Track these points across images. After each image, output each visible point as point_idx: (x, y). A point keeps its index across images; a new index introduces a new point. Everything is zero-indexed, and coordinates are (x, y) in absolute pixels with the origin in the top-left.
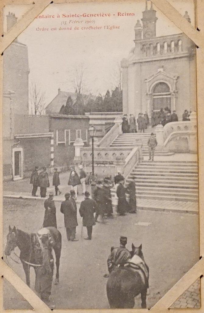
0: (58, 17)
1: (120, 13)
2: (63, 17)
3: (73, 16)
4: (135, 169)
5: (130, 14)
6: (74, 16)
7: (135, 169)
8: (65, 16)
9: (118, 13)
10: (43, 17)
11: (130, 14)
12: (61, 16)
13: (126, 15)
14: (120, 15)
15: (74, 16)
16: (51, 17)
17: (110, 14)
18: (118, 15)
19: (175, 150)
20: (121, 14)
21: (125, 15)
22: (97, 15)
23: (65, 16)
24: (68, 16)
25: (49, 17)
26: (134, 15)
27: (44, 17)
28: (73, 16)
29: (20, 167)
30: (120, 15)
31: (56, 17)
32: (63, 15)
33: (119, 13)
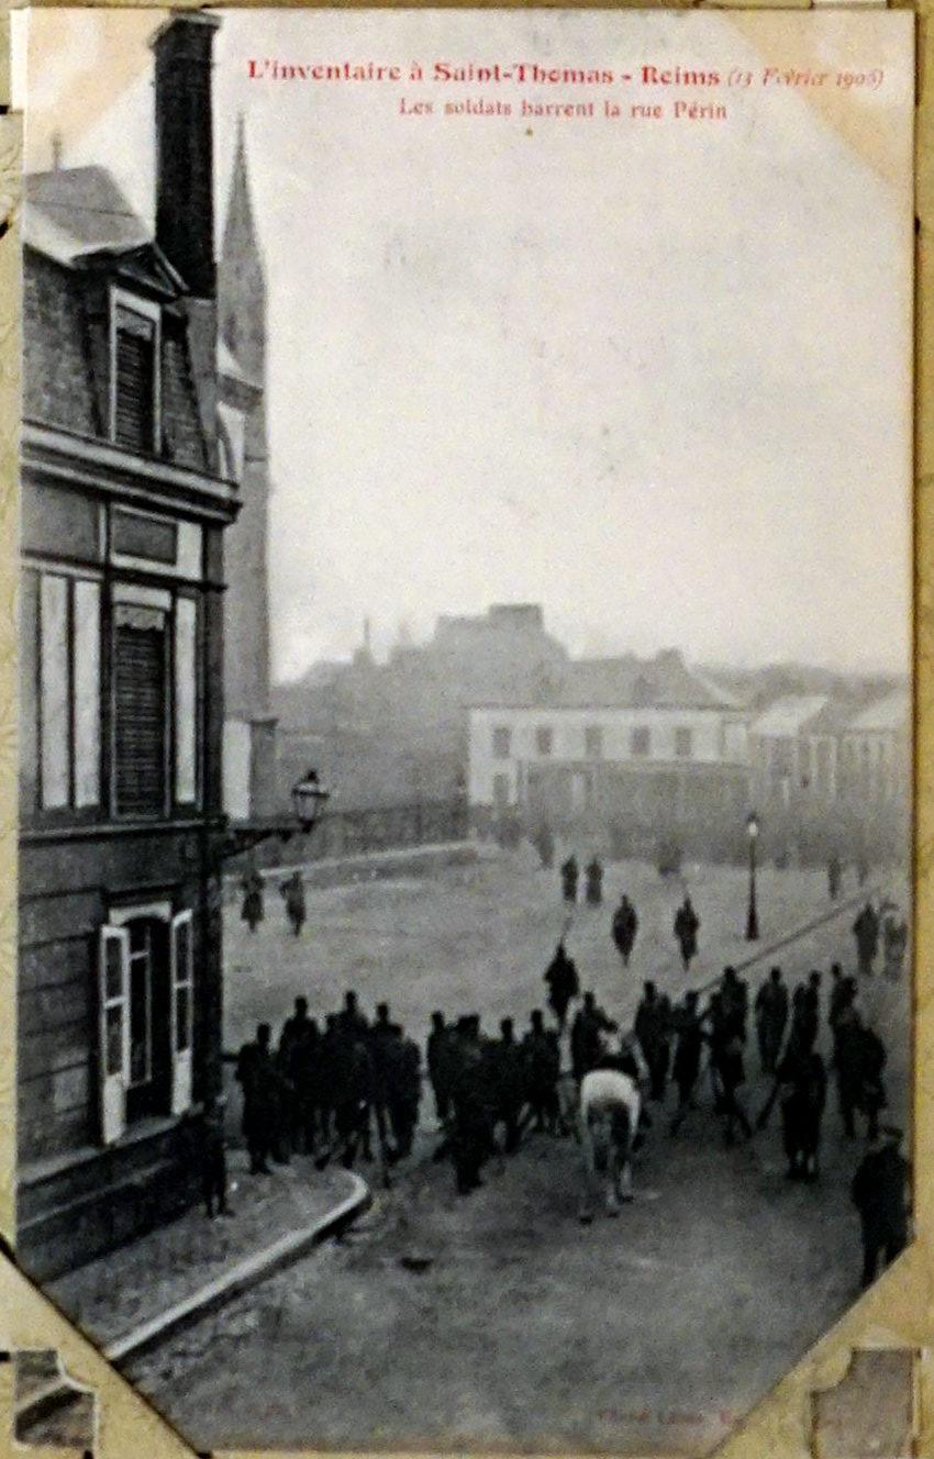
0: (413, 76)
1: (654, 70)
2: (437, 78)
3: (484, 75)
4: (297, 875)
5: (699, 79)
6: (488, 74)
7: (297, 875)
8: (448, 76)
9: (646, 70)
10: (347, 75)
11: (699, 79)
12: (429, 72)
13: (682, 79)
14: (655, 81)
15: (488, 74)
16: (385, 75)
17: (398, 70)
18: (646, 79)
19: (280, 817)
20: (658, 77)
21: (678, 81)
22: (301, 69)
23: (448, 76)
24: (460, 75)
25: (375, 74)
26: (611, 79)
27: (351, 73)
28: (484, 75)
29: (202, 788)
30: (655, 81)
31: (405, 73)
32: (438, 68)
33: (650, 72)
